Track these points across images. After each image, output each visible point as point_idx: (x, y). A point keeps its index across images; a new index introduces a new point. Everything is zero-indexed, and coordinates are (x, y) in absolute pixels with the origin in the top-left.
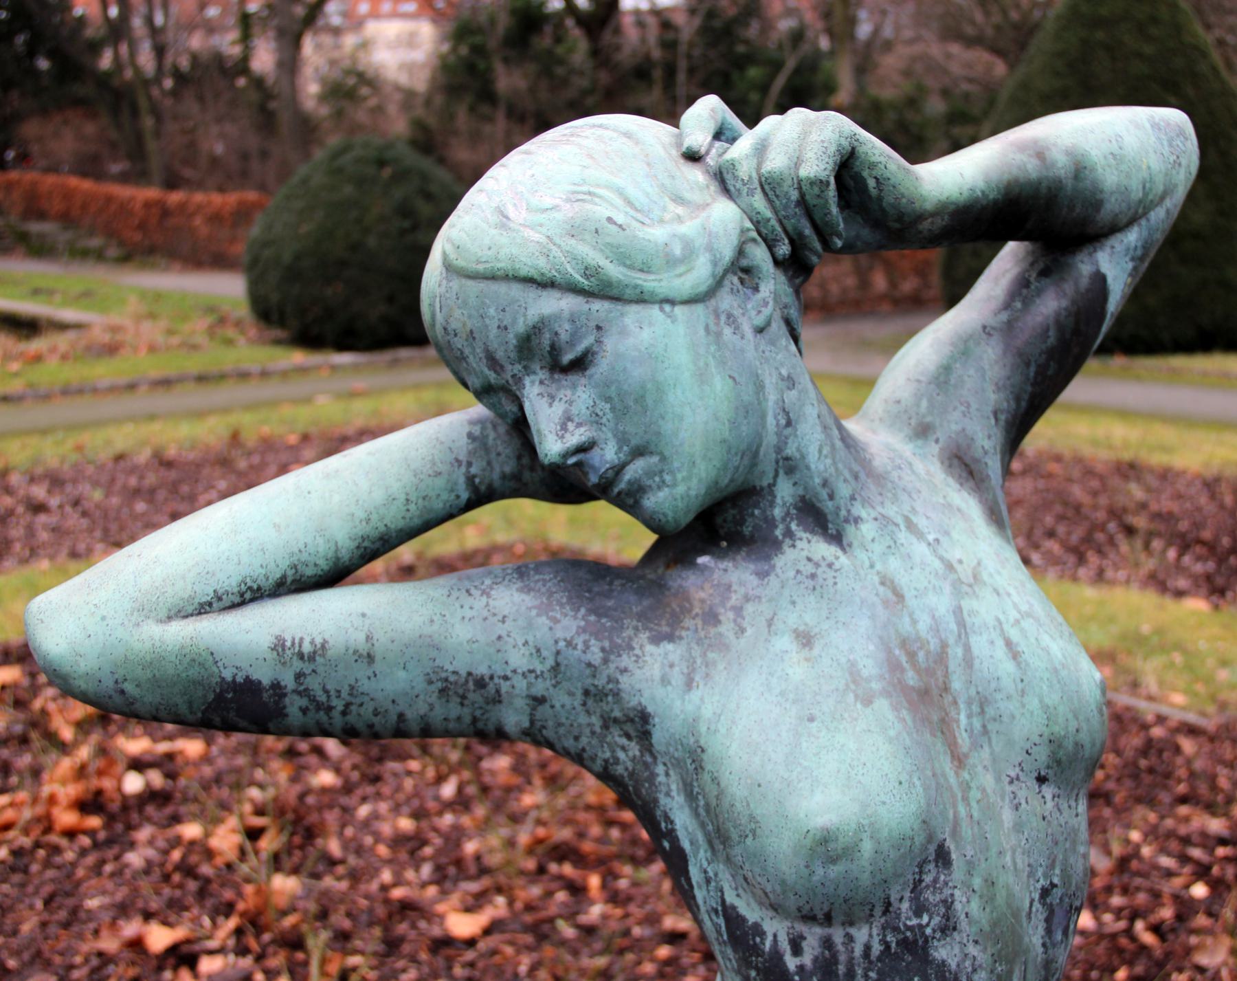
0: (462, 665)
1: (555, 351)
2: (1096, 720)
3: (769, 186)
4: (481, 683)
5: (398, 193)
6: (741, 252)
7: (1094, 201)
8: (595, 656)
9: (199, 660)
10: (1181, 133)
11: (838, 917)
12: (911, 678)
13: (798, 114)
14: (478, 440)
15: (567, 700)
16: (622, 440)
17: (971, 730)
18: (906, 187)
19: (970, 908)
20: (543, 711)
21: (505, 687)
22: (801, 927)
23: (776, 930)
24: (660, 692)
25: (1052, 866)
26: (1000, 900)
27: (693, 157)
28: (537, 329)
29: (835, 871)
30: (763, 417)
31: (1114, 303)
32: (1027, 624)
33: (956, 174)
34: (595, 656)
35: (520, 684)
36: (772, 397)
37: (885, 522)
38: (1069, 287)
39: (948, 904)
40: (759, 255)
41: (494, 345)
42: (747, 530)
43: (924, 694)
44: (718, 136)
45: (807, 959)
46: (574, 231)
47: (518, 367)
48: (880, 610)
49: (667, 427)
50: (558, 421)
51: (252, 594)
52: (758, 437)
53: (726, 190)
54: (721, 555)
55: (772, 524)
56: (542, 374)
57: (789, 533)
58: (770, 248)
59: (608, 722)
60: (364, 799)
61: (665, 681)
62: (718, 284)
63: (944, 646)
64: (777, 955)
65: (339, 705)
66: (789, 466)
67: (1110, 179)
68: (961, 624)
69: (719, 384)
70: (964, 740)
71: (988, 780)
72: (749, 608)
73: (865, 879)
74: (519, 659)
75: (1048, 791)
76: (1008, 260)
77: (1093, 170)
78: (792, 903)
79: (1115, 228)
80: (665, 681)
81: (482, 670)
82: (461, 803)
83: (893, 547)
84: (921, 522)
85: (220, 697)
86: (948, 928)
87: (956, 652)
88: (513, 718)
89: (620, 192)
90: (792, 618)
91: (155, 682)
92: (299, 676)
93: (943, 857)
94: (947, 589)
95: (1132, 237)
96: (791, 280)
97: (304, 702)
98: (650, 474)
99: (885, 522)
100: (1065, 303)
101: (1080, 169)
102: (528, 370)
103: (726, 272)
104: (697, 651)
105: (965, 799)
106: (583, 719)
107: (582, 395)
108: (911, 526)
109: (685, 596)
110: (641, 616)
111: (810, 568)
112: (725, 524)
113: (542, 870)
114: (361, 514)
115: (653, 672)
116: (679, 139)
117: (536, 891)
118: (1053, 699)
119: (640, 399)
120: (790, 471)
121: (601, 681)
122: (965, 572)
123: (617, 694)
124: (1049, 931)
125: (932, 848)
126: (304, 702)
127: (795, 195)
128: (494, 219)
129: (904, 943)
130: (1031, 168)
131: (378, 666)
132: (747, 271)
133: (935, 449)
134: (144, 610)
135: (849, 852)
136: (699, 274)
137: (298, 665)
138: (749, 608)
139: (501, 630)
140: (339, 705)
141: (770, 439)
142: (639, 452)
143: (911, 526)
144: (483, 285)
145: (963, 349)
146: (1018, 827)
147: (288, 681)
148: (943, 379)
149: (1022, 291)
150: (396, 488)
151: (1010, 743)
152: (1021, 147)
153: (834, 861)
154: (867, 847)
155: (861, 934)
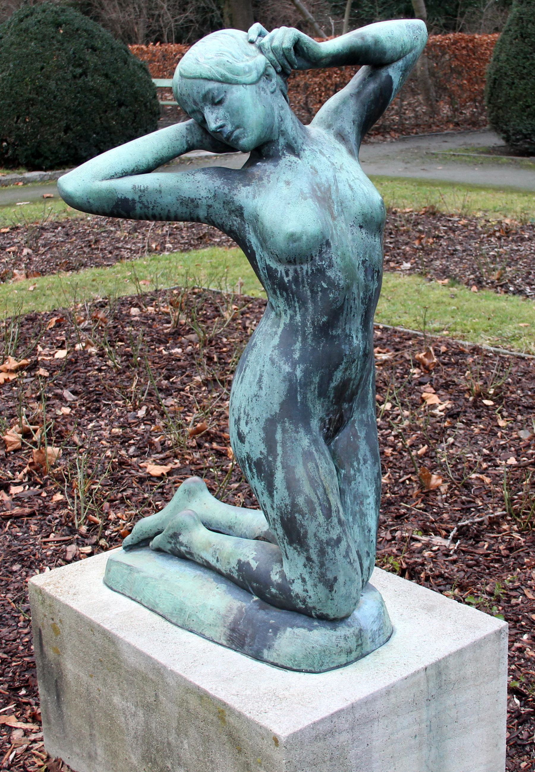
0: (187, 195)
1: (213, 98)
2: (379, 210)
3: (274, 50)
4: (192, 201)
5: (71, 47)
6: (266, 70)
7: (383, 52)
8: (226, 191)
9: (112, 192)
10: (419, 28)
11: (298, 261)
12: (319, 194)
13: (283, 28)
14: (189, 129)
15: (218, 206)
16: (233, 124)
17: (338, 211)
18: (316, 49)
19: (337, 260)
20: (211, 210)
21: (200, 202)
22: (288, 267)
23: (281, 268)
24: (246, 200)
25: (365, 254)
26: (347, 259)
27: (252, 42)
28: (208, 92)
29: (296, 244)
30: (274, 118)
31: (395, 86)
32: (356, 181)
33: (332, 45)
34: (226, 191)
35: (204, 201)
36: (276, 112)
37: (313, 151)
38: (378, 81)
39: (331, 259)
40: (272, 70)
41: (196, 98)
42: (271, 153)
43: (324, 199)
44: (260, 35)
45: (290, 278)
46: (218, 65)
47: (202, 104)
48: (310, 175)
49: (245, 120)
50: (214, 119)
51: (125, 174)
52: (272, 123)
53: (262, 52)
54: (264, 161)
55: (278, 151)
56: (210, 106)
57: (283, 154)
58: (275, 69)
59: (231, 212)
60: (91, 421)
61: (247, 197)
62: (259, 79)
63: (330, 186)
64: (282, 277)
65: (151, 206)
66: (283, 133)
67: (388, 45)
68: (335, 180)
69: (260, 108)
70: (336, 213)
71: (344, 225)
72: (272, 175)
73: (304, 248)
74: (204, 193)
75: (363, 231)
76: (362, 71)
77: (382, 42)
78: (284, 257)
79: (392, 61)
80: (247, 197)
81: (193, 196)
82: (149, 419)
83: (315, 158)
84: (325, 152)
85: (117, 203)
86: (331, 266)
87: (333, 188)
88: (202, 213)
89: (230, 53)
90: (284, 177)
91: (99, 199)
92: (140, 197)
93: (328, 244)
94: (332, 170)
95: (400, 63)
96: (282, 78)
97: (141, 205)
98: (241, 134)
99: (313, 151)
100: (376, 85)
101: (377, 42)
102: (205, 105)
103: (261, 76)
104: (256, 188)
105: (335, 229)
106: (223, 212)
107: (221, 111)
108: (321, 152)
109: (253, 175)
110: (240, 180)
111: (289, 163)
112: (263, 151)
113: (199, 446)
114: (155, 152)
115: (244, 195)
116: (248, 36)
117: (197, 455)
118: (364, 202)
119: (238, 112)
120: (283, 135)
121: (228, 198)
122: (338, 166)
123: (233, 202)
124: (366, 275)
125: (324, 241)
126: (141, 205)
127: (281, 53)
128: (195, 61)
129: (317, 270)
130: (359, 42)
131: (163, 194)
132: (268, 75)
133: (332, 132)
134: (95, 178)
135: (299, 239)
136: (253, 76)
137: (140, 194)
138: (272, 175)
139: (198, 185)
140: (151, 206)
141: (276, 124)
142: (238, 127)
143: (321, 152)
144: (192, 81)
145: (344, 102)
146: (353, 240)
147: (137, 199)
148: (337, 111)
149: (364, 83)
150: (165, 144)
151: (350, 215)
152: (356, 36)
153: (295, 241)
154: (304, 238)
155: (305, 267)
